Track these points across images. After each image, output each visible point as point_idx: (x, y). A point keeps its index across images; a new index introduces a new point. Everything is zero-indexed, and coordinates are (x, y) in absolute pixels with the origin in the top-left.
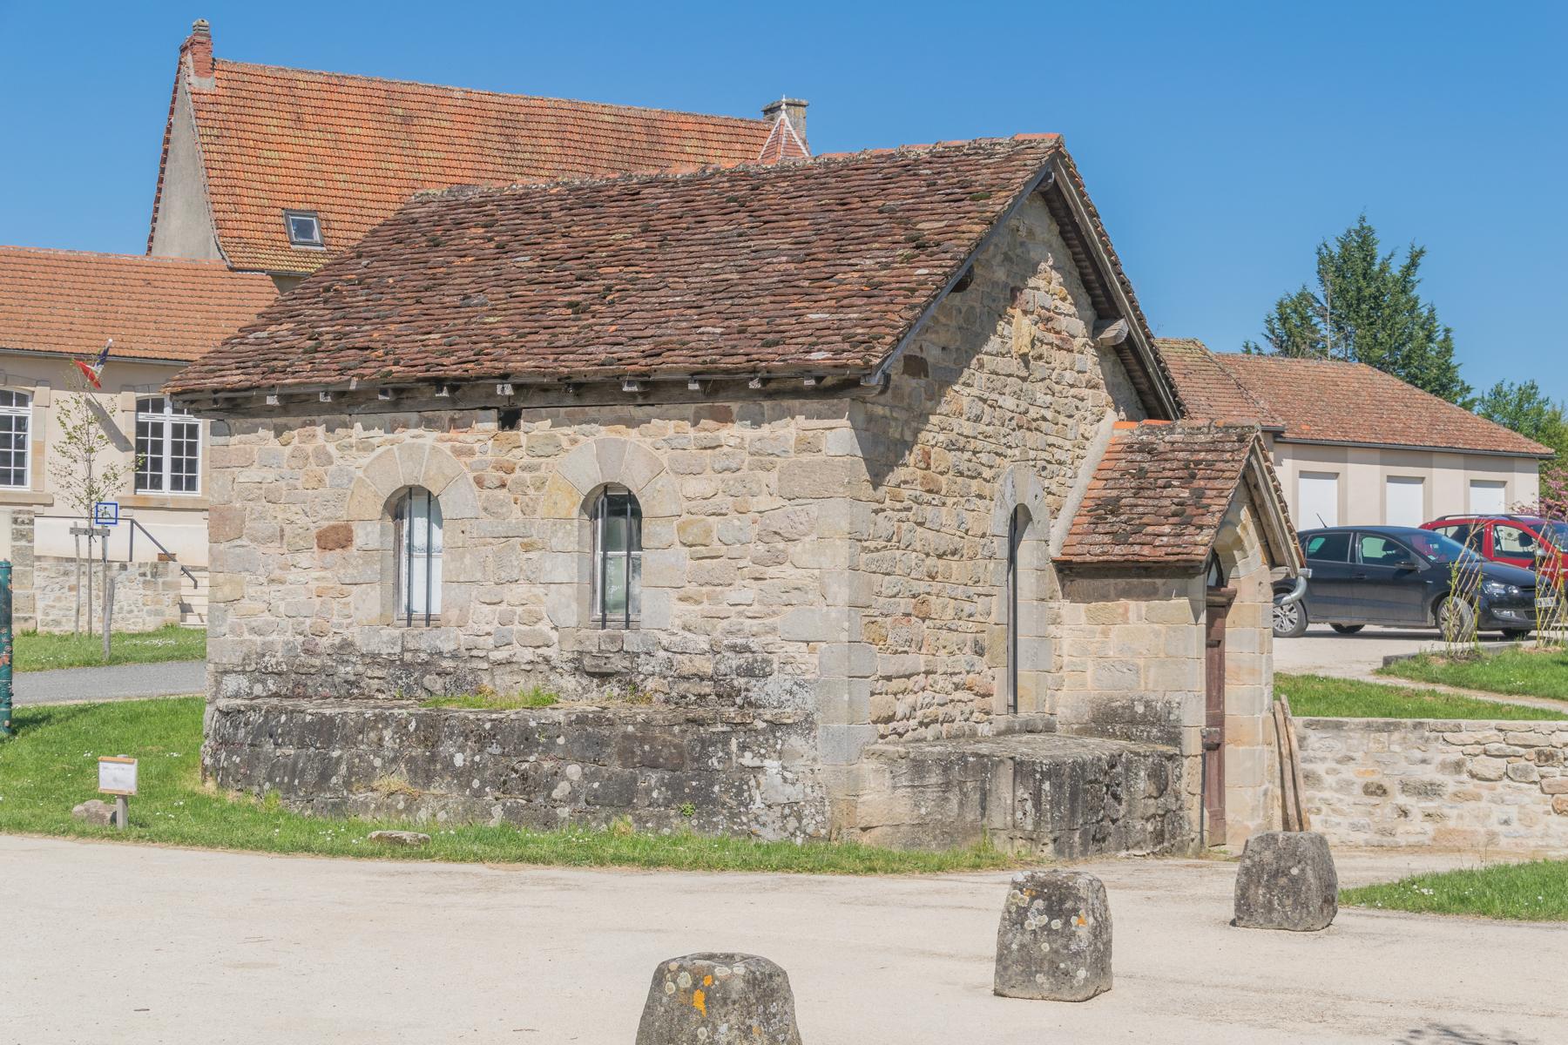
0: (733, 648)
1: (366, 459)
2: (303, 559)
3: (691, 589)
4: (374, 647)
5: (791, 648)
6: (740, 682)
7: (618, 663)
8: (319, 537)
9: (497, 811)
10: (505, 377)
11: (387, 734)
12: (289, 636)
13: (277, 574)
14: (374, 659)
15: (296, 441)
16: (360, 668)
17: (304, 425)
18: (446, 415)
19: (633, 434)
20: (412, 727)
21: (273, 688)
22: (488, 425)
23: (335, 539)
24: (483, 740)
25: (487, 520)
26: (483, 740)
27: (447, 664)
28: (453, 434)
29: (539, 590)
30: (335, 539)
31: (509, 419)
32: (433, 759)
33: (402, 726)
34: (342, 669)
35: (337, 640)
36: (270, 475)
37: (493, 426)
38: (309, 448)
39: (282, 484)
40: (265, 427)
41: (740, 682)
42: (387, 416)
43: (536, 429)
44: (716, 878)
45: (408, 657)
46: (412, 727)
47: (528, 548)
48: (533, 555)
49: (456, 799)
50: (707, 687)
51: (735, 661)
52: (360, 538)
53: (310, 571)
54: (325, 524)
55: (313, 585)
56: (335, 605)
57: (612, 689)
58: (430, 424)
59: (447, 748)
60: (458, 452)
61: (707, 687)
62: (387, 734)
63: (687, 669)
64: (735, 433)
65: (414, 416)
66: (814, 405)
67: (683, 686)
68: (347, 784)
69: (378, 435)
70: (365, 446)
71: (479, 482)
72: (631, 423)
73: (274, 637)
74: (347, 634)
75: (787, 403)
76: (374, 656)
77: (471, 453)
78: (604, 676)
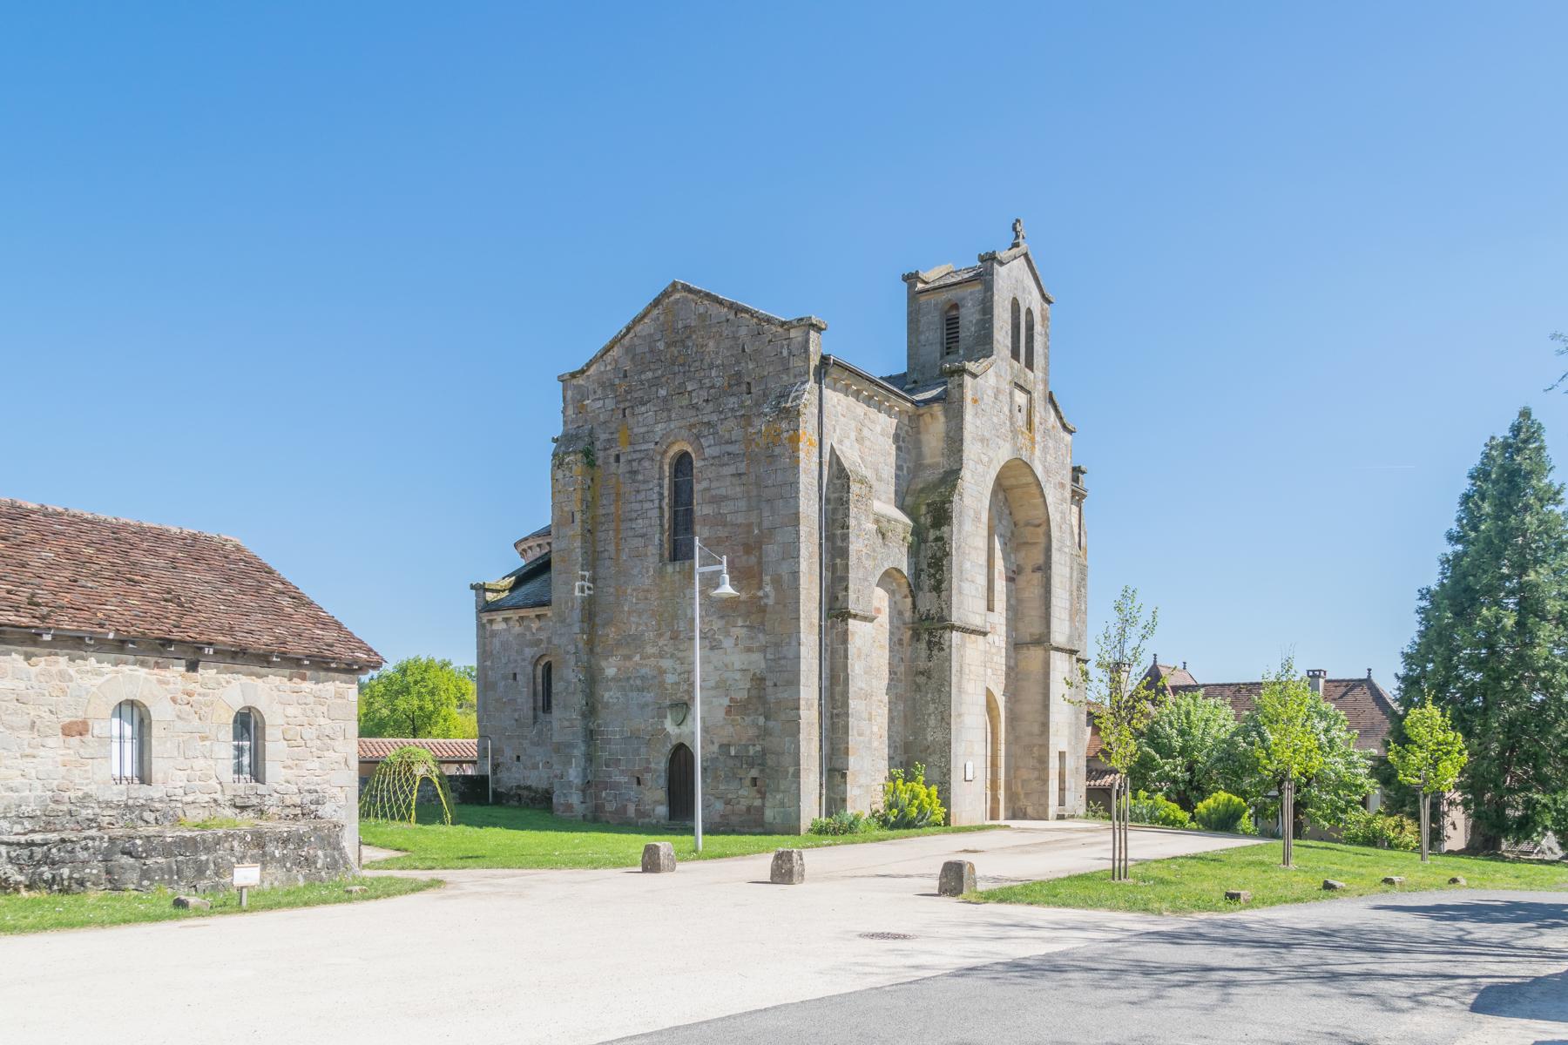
0: (309, 791)
1: (100, 680)
2: (50, 742)
3: (289, 762)
4: (108, 797)
5: (335, 790)
6: (313, 807)
7: (254, 801)
8: (63, 729)
9: (300, 877)
10: (210, 644)
11: (235, 844)
12: (39, 793)
13: (29, 751)
14: (108, 805)
15: (43, 664)
16: (98, 811)
17: (50, 654)
18: (152, 660)
19: (259, 682)
20: (249, 838)
21: (29, 827)
22: (180, 668)
23: (75, 729)
24: (286, 842)
25: (179, 724)
26: (286, 842)
27: (157, 805)
28: (156, 671)
29: (211, 762)
30: (75, 729)
31: (192, 667)
32: (264, 854)
33: (242, 839)
34: (84, 812)
35: (80, 794)
36: (22, 685)
37: (183, 669)
38: (54, 669)
39: (31, 692)
40: (17, 652)
41: (313, 807)
42: (113, 656)
43: (207, 673)
44: (601, 872)
45: (130, 802)
46: (249, 838)
47: (204, 739)
48: (208, 743)
49: (281, 873)
50: (298, 811)
51: (309, 797)
52: (97, 728)
53: (56, 750)
54: (68, 720)
55: (59, 759)
56: (76, 772)
57: (249, 814)
58: (143, 664)
59: (270, 848)
60: (160, 682)
61: (298, 811)
62: (235, 844)
63: (288, 802)
64: (307, 686)
65: (131, 658)
66: (343, 676)
67: (287, 811)
68: (217, 874)
69: (107, 667)
70: (99, 674)
71: (174, 700)
72: (260, 676)
73: (27, 793)
74: (86, 789)
75: (332, 674)
76: (107, 803)
77: (168, 683)
78: (243, 808)
